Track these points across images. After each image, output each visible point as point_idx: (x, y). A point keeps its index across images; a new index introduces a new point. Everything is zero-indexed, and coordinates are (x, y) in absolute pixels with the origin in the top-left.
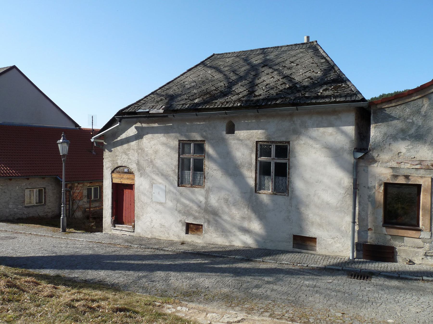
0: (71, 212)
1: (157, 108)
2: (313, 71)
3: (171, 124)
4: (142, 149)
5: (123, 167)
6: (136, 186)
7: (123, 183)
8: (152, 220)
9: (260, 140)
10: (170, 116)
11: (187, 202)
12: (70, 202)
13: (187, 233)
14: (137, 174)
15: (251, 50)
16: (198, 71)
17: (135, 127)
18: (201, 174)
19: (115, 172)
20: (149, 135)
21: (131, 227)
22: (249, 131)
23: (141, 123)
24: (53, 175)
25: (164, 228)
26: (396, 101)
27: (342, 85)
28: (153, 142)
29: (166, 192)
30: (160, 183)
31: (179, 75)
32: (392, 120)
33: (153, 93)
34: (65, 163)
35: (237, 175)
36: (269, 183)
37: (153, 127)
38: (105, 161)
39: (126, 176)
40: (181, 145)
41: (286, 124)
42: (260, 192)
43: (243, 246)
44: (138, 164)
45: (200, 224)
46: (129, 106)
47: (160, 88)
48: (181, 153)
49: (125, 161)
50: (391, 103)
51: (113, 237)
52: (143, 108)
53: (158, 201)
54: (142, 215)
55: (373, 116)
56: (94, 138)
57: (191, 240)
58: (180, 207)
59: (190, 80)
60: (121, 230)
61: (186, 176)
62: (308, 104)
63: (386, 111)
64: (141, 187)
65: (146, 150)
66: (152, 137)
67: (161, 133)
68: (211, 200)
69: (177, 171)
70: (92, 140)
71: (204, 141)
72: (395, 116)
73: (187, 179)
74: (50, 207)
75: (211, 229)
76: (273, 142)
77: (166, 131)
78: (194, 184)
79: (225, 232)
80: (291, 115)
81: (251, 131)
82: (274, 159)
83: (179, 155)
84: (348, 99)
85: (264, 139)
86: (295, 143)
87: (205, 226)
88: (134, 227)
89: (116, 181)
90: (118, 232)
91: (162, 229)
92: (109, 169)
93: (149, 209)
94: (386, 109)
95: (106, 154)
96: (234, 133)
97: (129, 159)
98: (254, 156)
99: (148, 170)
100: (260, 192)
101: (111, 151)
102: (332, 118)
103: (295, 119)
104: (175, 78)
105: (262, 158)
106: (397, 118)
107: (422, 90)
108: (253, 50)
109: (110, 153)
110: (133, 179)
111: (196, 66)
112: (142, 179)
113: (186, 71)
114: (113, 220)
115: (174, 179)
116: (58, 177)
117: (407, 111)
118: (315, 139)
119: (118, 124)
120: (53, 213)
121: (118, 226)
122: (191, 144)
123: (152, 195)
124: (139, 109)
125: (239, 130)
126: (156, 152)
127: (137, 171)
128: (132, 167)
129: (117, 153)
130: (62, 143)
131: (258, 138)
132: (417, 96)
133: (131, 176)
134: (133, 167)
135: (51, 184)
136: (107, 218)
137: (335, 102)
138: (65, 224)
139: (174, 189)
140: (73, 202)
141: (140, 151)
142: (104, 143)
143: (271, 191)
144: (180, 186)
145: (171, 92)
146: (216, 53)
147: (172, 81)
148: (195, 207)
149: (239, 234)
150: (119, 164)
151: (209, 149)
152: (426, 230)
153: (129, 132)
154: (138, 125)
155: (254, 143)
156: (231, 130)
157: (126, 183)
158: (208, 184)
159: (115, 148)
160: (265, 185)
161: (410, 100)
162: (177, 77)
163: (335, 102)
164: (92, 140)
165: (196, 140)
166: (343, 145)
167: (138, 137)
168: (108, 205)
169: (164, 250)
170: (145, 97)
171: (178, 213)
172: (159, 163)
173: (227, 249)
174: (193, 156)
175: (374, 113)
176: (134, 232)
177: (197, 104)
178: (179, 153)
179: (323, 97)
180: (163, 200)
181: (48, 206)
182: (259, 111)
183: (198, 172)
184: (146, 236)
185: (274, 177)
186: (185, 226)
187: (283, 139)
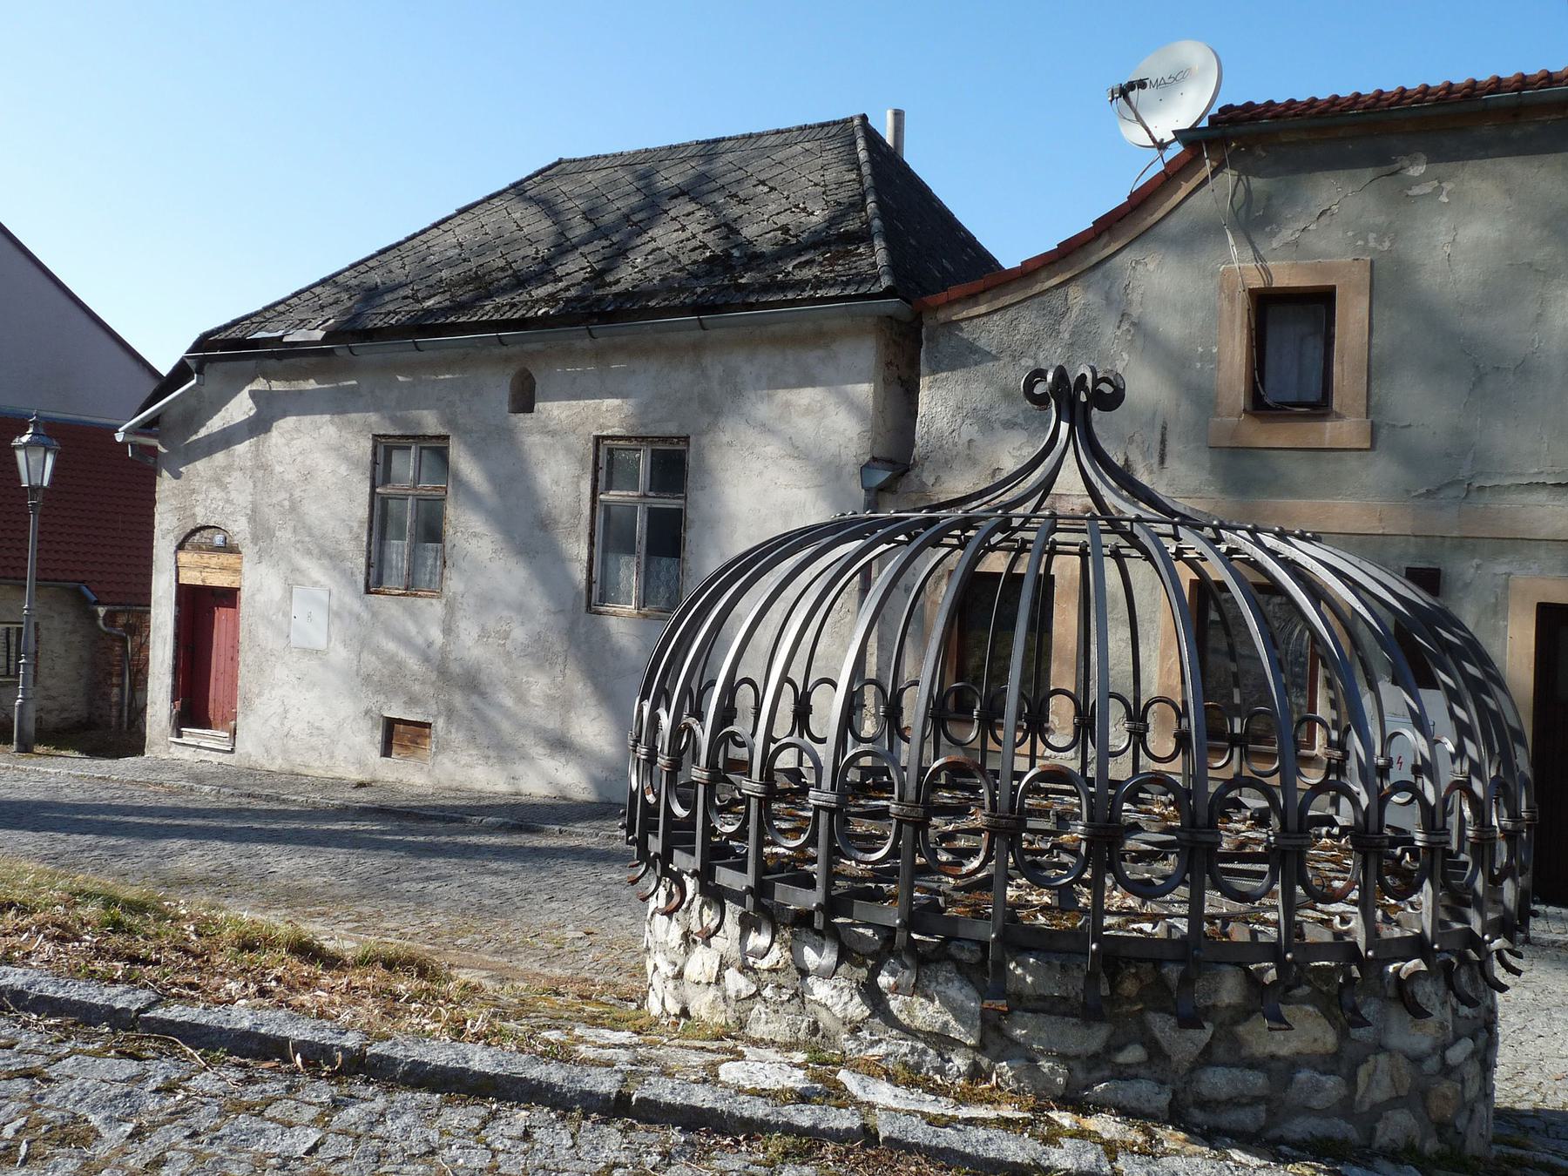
0: (126, 714)
1: (309, 326)
2: (804, 210)
3: (354, 382)
4: (265, 467)
5: (209, 530)
6: (244, 596)
7: (208, 583)
8: (286, 711)
9: (605, 433)
10: (341, 350)
11: (390, 646)
12: (123, 680)
13: (387, 752)
14: (248, 551)
15: (670, 147)
16: (488, 213)
17: (250, 391)
18: (437, 552)
19: (187, 546)
20: (288, 418)
21: (227, 735)
22: (574, 403)
23: (268, 377)
24: (65, 581)
25: (321, 737)
26: (989, 295)
27: (858, 248)
28: (299, 441)
29: (334, 615)
30: (315, 584)
31: (427, 225)
32: (980, 363)
33: (323, 282)
34: (37, 517)
35: (537, 553)
36: (629, 575)
37: (301, 392)
38: (159, 509)
39: (215, 560)
40: (381, 451)
41: (682, 378)
42: (602, 609)
43: (544, 792)
44: (254, 516)
45: (422, 720)
46: (235, 323)
47: (353, 266)
48: (379, 480)
49: (216, 509)
50: (977, 304)
51: (172, 766)
52: (270, 326)
53: (306, 645)
54: (260, 695)
55: (928, 348)
56: (126, 432)
57: (396, 775)
58: (371, 662)
59: (445, 243)
60: (199, 747)
61: (394, 556)
62: (750, 307)
63: (962, 330)
64: (258, 597)
65: (278, 469)
66: (297, 423)
67: (322, 413)
68: (458, 637)
69: (365, 539)
70: (119, 437)
71: (446, 438)
72: (987, 349)
73: (397, 568)
74: (53, 693)
75: (457, 737)
76: (643, 438)
77: (337, 405)
78: (411, 588)
79: (502, 751)
80: (697, 348)
81: (582, 403)
82: (645, 496)
83: (373, 487)
84: (850, 291)
85: (616, 429)
86: (705, 440)
87: (439, 729)
88: (234, 733)
89: (191, 578)
90: (187, 755)
91: (314, 741)
92: (171, 536)
93: (280, 673)
94: (963, 324)
95: (165, 485)
96: (531, 411)
97: (227, 501)
98: (586, 487)
99: (284, 535)
100: (602, 609)
101: (177, 476)
102: (812, 357)
103: (707, 360)
104: (409, 234)
105: (611, 492)
106: (994, 352)
107: (1064, 257)
108: (675, 147)
109: (175, 482)
110: (237, 571)
111: (492, 197)
112: (263, 568)
113: (452, 212)
114: (174, 712)
115: (355, 569)
116: (84, 589)
117: (1022, 330)
118: (765, 428)
119: (193, 382)
120: (65, 715)
121: (192, 735)
122: (410, 448)
123: (289, 623)
124: (260, 330)
125: (546, 400)
126: (307, 476)
127: (248, 542)
128: (236, 529)
129: (195, 484)
130: (25, 446)
131: (601, 427)
132: (1049, 278)
133: (226, 559)
134: (239, 528)
135: (62, 613)
136: (157, 707)
137: (813, 300)
138: (31, 727)
139: (351, 600)
140: (135, 680)
141: (260, 474)
142: (161, 449)
143: (633, 607)
144: (372, 593)
145: (376, 278)
146: (566, 156)
147: (400, 244)
148: (413, 663)
149: (538, 751)
150: (201, 521)
151: (464, 462)
152: (1063, 728)
153: (230, 411)
154: (260, 385)
155: (590, 444)
156: (524, 401)
157: (216, 583)
158: (454, 584)
159: (190, 466)
160: (618, 584)
161: (1031, 293)
162: (417, 230)
163: (813, 300)
164: (119, 437)
165: (424, 436)
166: (840, 446)
167: (258, 426)
168: (163, 661)
169: (284, 800)
170: (296, 295)
171: (363, 685)
172: (314, 512)
173: (497, 801)
174: (415, 487)
175: (930, 339)
176: (232, 751)
177: (429, 312)
178: (373, 479)
179: (800, 285)
180: (320, 641)
181: (46, 689)
182: (593, 331)
183: (430, 545)
184: (268, 766)
185: (643, 558)
186: (381, 728)
187: (671, 429)
